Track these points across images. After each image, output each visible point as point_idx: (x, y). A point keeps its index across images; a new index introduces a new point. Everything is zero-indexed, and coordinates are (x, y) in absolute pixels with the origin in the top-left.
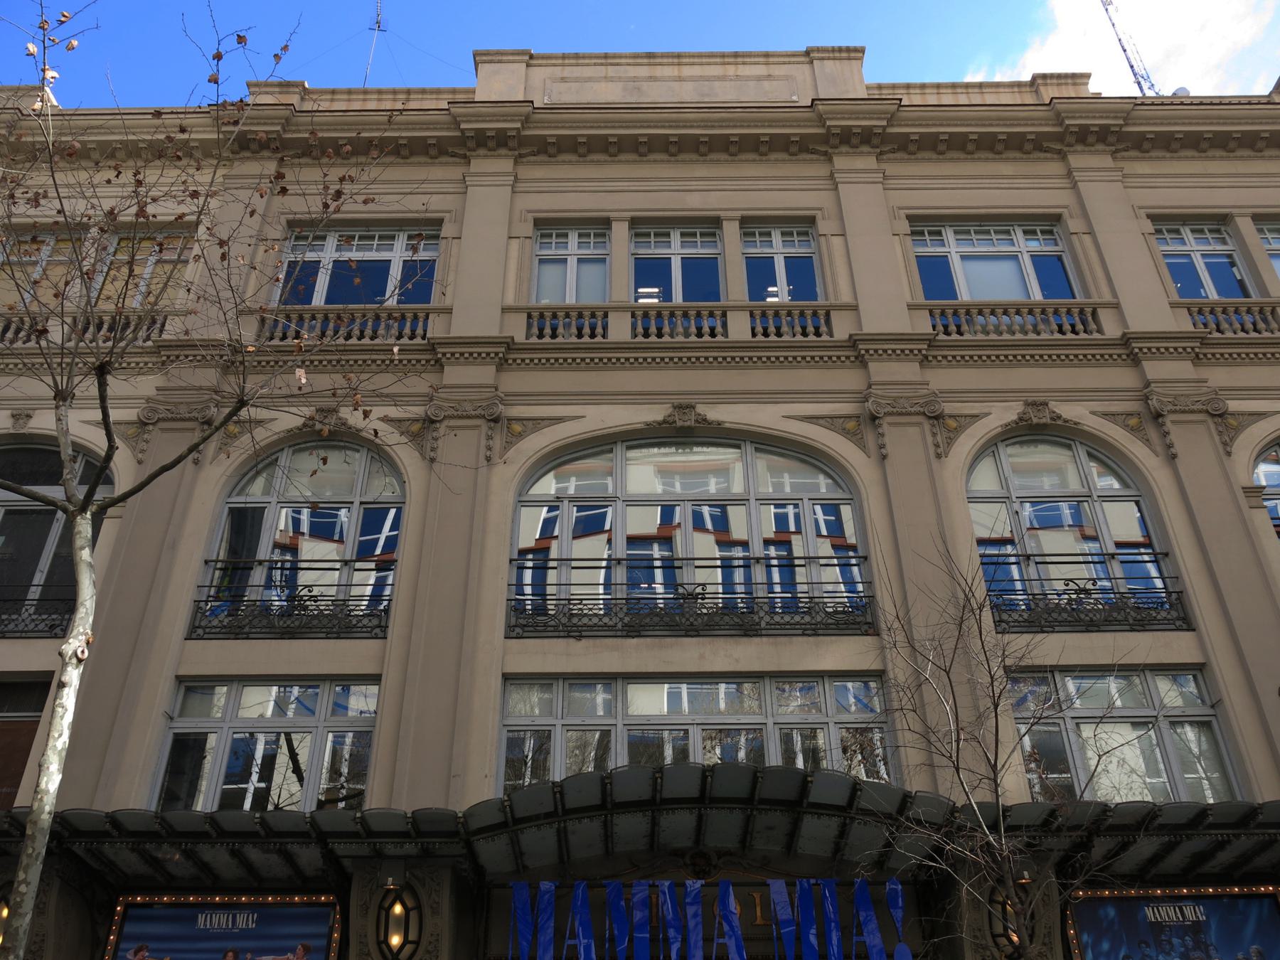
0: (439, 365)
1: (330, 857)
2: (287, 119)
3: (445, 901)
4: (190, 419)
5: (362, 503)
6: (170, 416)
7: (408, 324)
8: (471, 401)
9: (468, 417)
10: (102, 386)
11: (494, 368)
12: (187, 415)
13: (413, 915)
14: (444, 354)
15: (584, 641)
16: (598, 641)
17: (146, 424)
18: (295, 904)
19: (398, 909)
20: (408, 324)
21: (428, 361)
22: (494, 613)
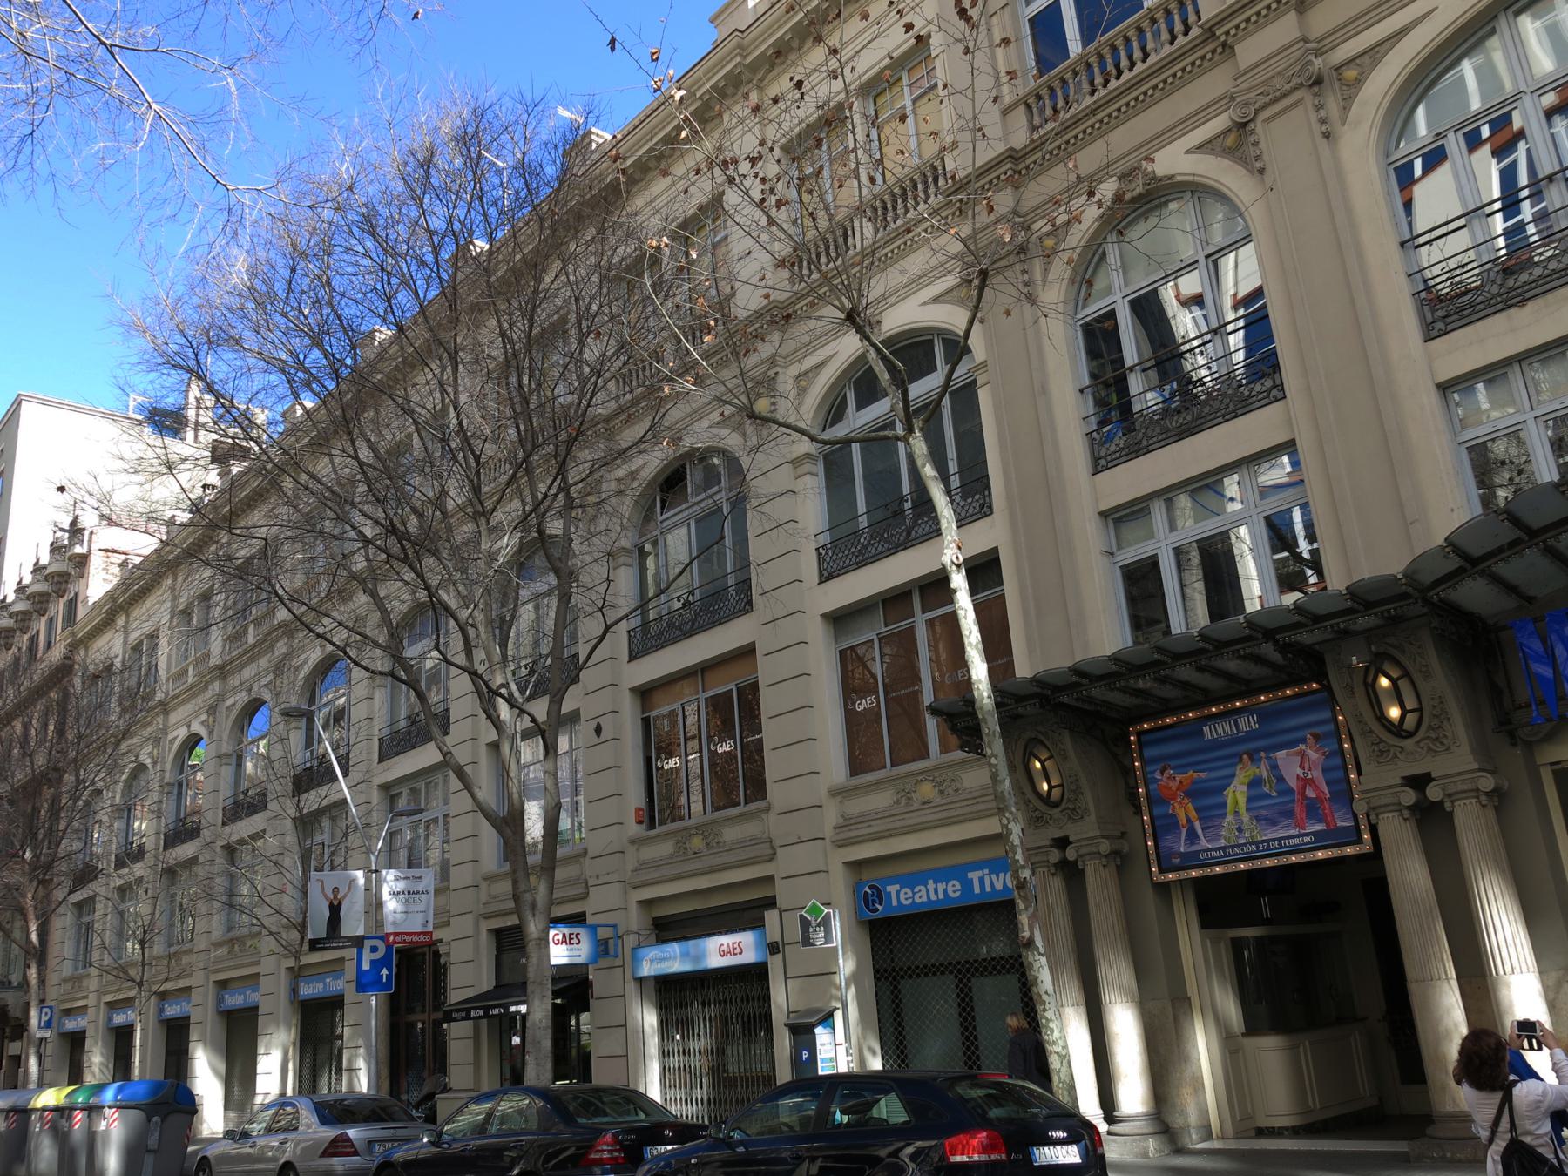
0: (1227, 49)
1: (1284, 648)
2: (739, 46)
3: (1433, 660)
4: (1294, 89)
5: (1207, 257)
6: (1267, 99)
7: (1177, 17)
8: (1279, 73)
9: (1284, 96)
10: (373, 594)
11: (1009, 189)
12: (1287, 87)
13: (1404, 685)
14: (1227, 33)
15: (1530, 306)
16: (1550, 296)
17: (1246, 124)
18: (1289, 698)
19: (1384, 682)
20: (1177, 17)
21: (1214, 51)
22: (1402, 317)
